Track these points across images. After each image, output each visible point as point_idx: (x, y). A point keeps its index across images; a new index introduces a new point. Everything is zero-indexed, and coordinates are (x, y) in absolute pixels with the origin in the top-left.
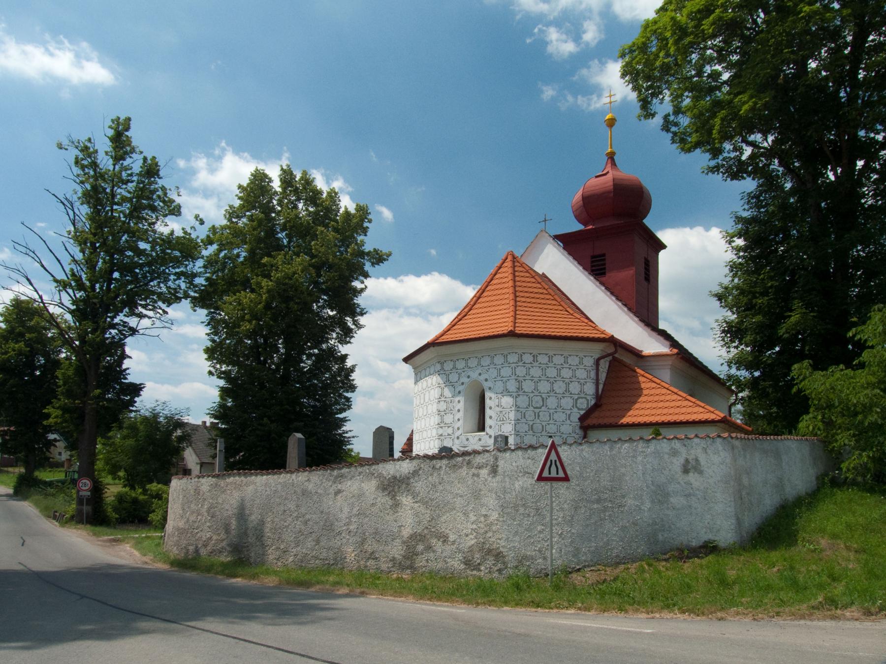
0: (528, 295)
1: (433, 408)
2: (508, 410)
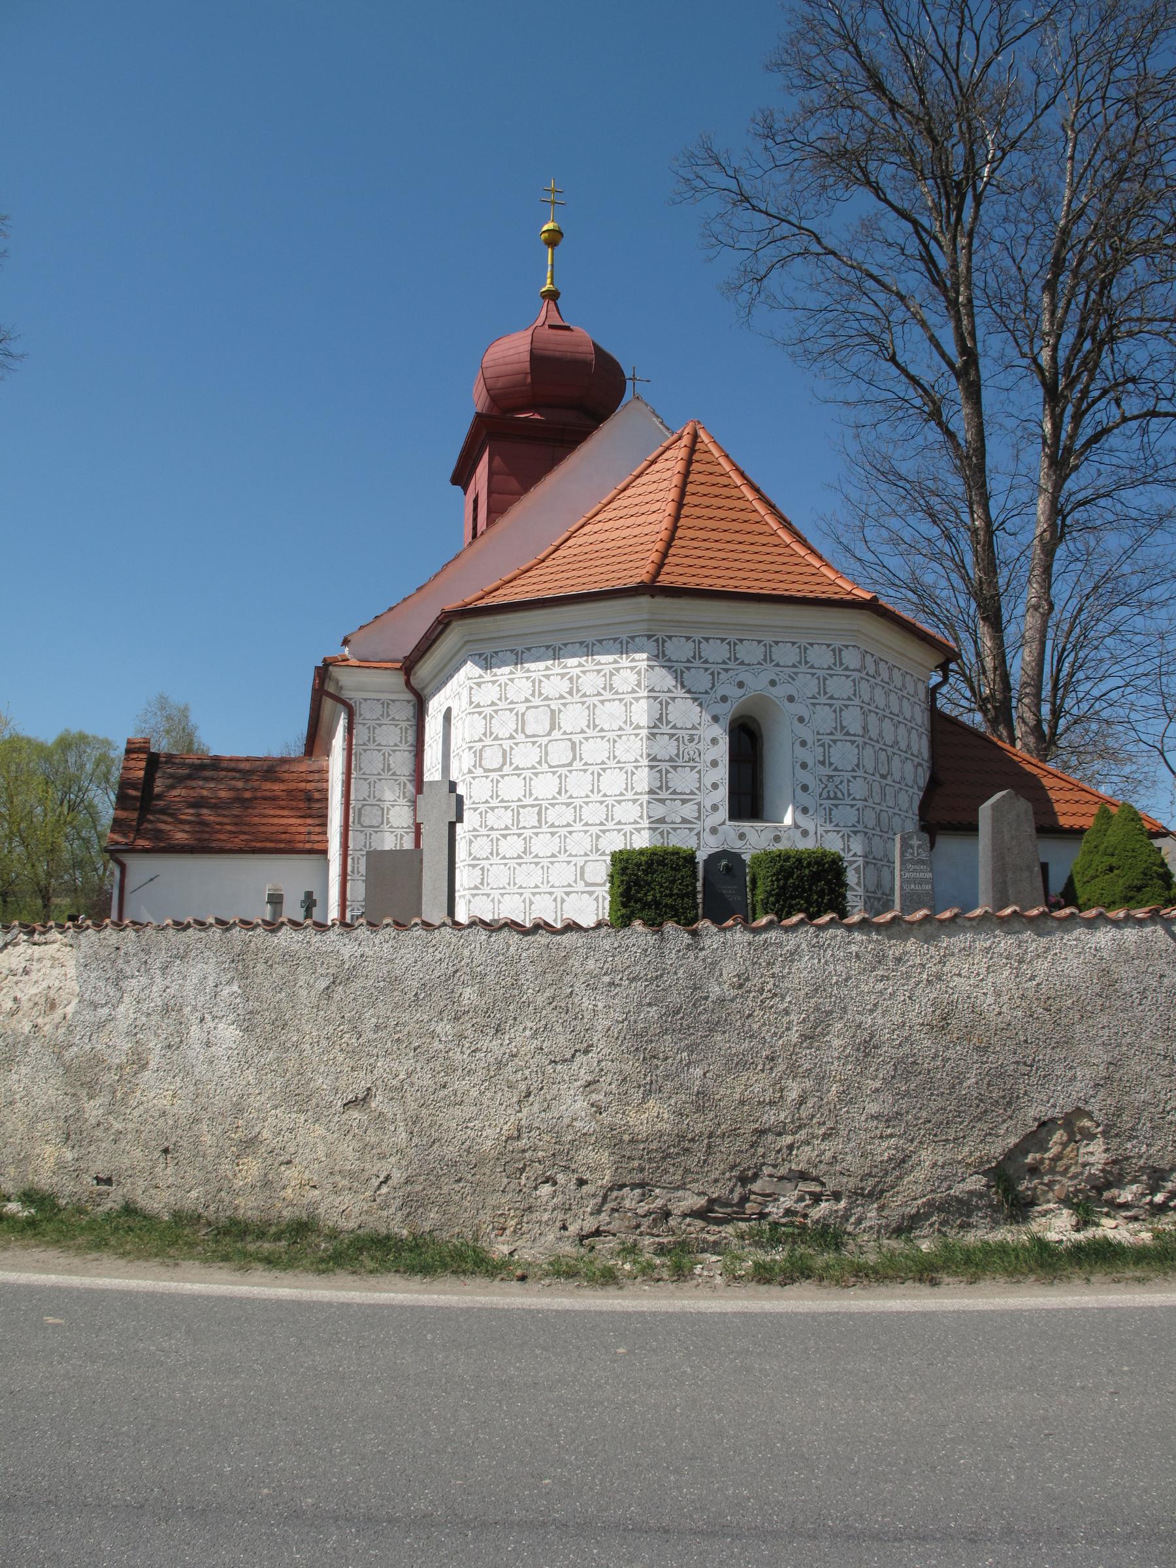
0: (736, 526)
1: (634, 748)
2: (848, 775)
